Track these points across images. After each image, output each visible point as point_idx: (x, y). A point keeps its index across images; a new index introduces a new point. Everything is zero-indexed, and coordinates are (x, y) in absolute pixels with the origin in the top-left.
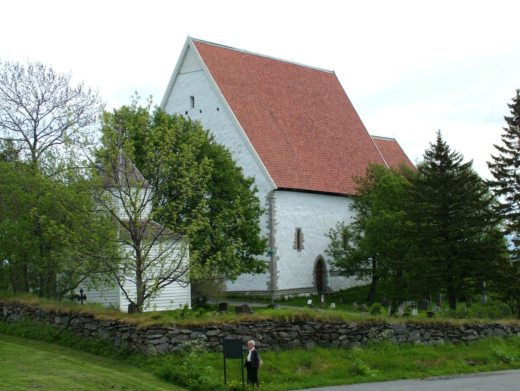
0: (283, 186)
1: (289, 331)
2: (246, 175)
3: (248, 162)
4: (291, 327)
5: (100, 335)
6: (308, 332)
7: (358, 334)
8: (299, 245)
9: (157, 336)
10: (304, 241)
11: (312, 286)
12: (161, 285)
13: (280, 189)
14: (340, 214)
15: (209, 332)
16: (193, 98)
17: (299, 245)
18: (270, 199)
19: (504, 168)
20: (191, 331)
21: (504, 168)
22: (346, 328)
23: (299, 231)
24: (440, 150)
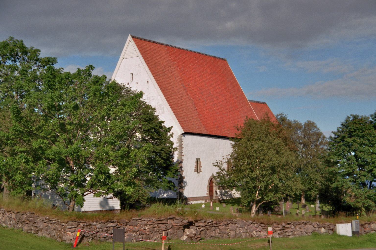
0: (188, 131)
1: (165, 224)
2: (167, 125)
3: (166, 116)
4: (167, 221)
5: (39, 225)
6: (179, 224)
7: (213, 227)
8: (198, 169)
9: (73, 226)
10: (201, 167)
11: (207, 195)
12: (85, 194)
13: (186, 133)
14: (224, 149)
15: (110, 224)
16: (132, 74)
17: (198, 169)
18: (180, 140)
19: (355, 180)
20: (98, 224)
21: (355, 180)
22: (205, 222)
23: (198, 160)
24: (308, 121)
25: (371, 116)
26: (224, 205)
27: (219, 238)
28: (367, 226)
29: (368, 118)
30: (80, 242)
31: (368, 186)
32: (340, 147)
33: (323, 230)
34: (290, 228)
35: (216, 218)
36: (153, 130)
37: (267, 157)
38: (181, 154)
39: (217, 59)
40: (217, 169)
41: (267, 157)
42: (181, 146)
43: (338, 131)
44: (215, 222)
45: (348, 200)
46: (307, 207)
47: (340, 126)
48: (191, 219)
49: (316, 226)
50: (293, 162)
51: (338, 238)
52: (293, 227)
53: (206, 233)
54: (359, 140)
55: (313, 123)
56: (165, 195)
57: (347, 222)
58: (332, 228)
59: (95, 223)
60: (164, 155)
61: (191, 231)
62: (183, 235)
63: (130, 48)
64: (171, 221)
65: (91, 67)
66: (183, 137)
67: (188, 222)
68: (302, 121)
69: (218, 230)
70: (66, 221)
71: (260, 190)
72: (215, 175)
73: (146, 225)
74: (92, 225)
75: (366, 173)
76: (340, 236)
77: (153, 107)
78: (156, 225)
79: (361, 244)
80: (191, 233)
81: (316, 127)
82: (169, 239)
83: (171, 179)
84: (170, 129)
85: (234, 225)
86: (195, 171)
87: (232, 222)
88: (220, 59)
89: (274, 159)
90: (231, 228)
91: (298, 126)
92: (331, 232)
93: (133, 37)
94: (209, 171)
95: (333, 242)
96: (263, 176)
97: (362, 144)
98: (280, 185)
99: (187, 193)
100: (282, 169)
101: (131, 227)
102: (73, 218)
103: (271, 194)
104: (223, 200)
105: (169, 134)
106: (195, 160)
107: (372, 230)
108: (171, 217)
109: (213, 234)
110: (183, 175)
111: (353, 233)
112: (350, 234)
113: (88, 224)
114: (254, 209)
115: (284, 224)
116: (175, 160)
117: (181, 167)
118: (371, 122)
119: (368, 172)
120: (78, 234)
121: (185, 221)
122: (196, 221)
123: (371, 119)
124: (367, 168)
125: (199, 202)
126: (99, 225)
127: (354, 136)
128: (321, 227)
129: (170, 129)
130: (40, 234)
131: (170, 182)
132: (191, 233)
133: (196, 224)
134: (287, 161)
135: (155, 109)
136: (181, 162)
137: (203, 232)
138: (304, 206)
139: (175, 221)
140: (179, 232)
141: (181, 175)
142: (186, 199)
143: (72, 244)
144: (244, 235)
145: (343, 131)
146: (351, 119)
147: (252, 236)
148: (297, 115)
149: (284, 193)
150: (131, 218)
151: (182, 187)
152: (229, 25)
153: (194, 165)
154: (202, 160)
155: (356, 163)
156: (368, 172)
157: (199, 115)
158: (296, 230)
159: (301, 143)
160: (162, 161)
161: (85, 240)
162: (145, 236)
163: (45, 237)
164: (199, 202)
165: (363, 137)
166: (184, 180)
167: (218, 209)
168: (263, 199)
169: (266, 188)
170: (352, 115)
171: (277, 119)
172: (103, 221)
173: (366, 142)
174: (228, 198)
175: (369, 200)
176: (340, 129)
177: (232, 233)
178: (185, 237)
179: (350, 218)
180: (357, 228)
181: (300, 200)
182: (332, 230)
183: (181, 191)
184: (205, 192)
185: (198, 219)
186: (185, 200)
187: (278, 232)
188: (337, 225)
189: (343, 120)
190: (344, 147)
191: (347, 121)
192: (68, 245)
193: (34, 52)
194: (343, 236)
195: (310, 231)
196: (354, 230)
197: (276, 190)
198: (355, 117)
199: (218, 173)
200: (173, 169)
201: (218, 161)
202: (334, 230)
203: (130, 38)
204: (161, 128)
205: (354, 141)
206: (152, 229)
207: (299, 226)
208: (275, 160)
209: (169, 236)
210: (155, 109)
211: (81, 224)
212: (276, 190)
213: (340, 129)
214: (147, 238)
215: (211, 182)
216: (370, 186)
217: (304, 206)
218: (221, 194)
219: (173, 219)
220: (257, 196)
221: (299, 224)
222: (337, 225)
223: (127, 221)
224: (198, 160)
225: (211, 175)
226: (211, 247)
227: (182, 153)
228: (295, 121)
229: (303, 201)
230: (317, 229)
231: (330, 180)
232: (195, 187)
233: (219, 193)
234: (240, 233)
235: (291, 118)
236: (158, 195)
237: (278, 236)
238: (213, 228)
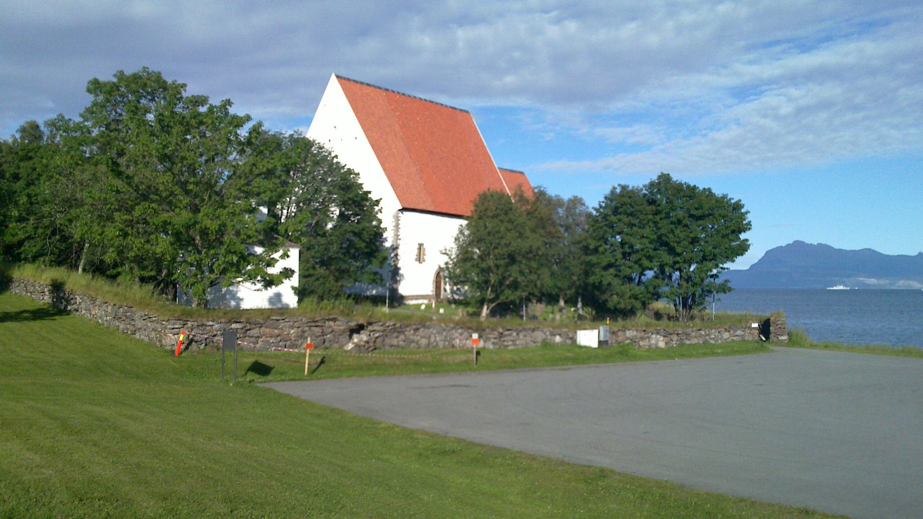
8: (420, 258)
11: (431, 293)
13: (404, 209)
17: (420, 258)
23: (421, 245)
25: (645, 186)
26: (453, 306)
27: (403, 348)
28: (620, 333)
29: (642, 190)
30: (187, 348)
31: (637, 281)
32: (601, 228)
33: (558, 339)
34: (510, 335)
35: (401, 320)
36: (350, 202)
37: (503, 242)
38: (397, 237)
39: (457, 112)
40: (446, 259)
41: (503, 242)
42: (397, 227)
43: (601, 206)
44: (398, 325)
45: (613, 301)
46: (564, 311)
47: (603, 199)
48: (361, 321)
49: (548, 333)
50: (539, 248)
51: (577, 350)
52: (515, 334)
53: (383, 341)
54: (626, 219)
55: (581, 199)
56: (374, 292)
57: (592, 328)
58: (571, 335)
59: (211, 323)
60: (366, 236)
61: (363, 337)
62: (349, 342)
63: (334, 92)
64: (331, 323)
65: (229, 103)
66: (400, 214)
67: (357, 325)
68: (566, 196)
69: (402, 337)
70: (167, 318)
71: (493, 286)
72: (443, 266)
73: (292, 327)
74: (206, 326)
75: (632, 264)
76: (580, 347)
77: (356, 171)
78: (306, 329)
79: (607, 359)
80: (361, 340)
81: (584, 204)
82: (327, 348)
83: (378, 270)
84: (378, 202)
85: (427, 331)
86: (416, 260)
87: (424, 326)
88: (461, 110)
89: (514, 244)
90: (422, 334)
91: (559, 203)
92: (569, 342)
93: (338, 77)
94: (436, 260)
95: (569, 354)
96: (497, 267)
97: (631, 225)
98: (519, 279)
99: (404, 289)
100: (524, 256)
101: (268, 330)
102: (176, 315)
103: (508, 292)
104: (454, 299)
105: (377, 208)
106: (417, 246)
107: (628, 338)
108: (331, 317)
109: (395, 342)
110: (399, 266)
111: (600, 342)
112: (595, 344)
113: (200, 323)
114: (485, 311)
115: (501, 330)
116: (388, 244)
117: (396, 255)
118: (645, 195)
119: (636, 262)
120: (182, 337)
121: (353, 324)
122: (370, 324)
123: (644, 191)
124: (634, 257)
125: (420, 301)
126: (216, 326)
127: (620, 214)
128: (555, 335)
129: (378, 202)
130: (137, 336)
131: (375, 273)
132: (361, 340)
133: (370, 328)
134: (531, 246)
135: (358, 174)
136: (397, 248)
137: (378, 340)
138: (561, 310)
139: (337, 323)
140: (343, 339)
141: (396, 266)
142: (402, 298)
143: (173, 351)
144: (441, 344)
145: (605, 208)
146: (618, 191)
147: (453, 346)
148: (560, 189)
149: (524, 291)
150: (269, 317)
151: (397, 282)
152: (510, 79)
153: (416, 252)
154: (424, 248)
155: (621, 250)
156: (636, 262)
157: (425, 185)
158: (518, 339)
159: (562, 226)
160: (364, 245)
161: (194, 346)
162: (288, 343)
163: (142, 340)
164: (420, 301)
165: (631, 214)
166: (401, 272)
167: (442, 311)
168: (497, 297)
169: (501, 283)
170: (619, 185)
171: (535, 193)
172: (223, 320)
173: (636, 222)
174: (462, 298)
175: (633, 300)
176: (603, 205)
177: (424, 342)
178: (350, 346)
179: (598, 323)
180: (605, 336)
181: (558, 301)
182: (571, 338)
183: (395, 286)
184: (429, 289)
185: (372, 320)
186: (396, 299)
187: (493, 340)
188: (578, 332)
189: (607, 191)
190: (605, 228)
191: (613, 192)
192: (167, 351)
193: (176, 87)
194: (585, 347)
195: (540, 339)
196: (602, 339)
197: (515, 286)
198: (624, 188)
199: (446, 263)
200: (380, 256)
201: (448, 248)
202: (573, 340)
203: (333, 81)
204: (367, 199)
205: (620, 220)
206: (300, 334)
207: (524, 333)
208: (517, 245)
209: (327, 344)
210: (358, 174)
211: (189, 324)
212: (515, 286)
213: (603, 205)
214: (291, 347)
215: (438, 275)
216: (639, 281)
217: (561, 310)
218: (452, 292)
219: (334, 320)
220: (489, 294)
221: (524, 329)
222: (578, 332)
223: (261, 321)
224: (421, 245)
225: (437, 267)
226: (386, 360)
227: (398, 236)
228: (556, 196)
229: (562, 303)
230: (549, 337)
231: (587, 274)
232: (416, 281)
233: (449, 291)
234: (435, 340)
235: (552, 192)
236: (365, 292)
237: (491, 347)
238: (396, 334)
